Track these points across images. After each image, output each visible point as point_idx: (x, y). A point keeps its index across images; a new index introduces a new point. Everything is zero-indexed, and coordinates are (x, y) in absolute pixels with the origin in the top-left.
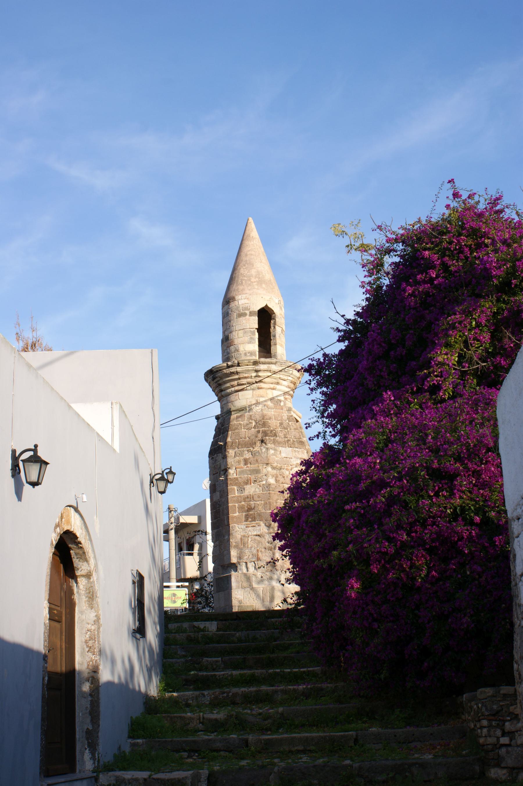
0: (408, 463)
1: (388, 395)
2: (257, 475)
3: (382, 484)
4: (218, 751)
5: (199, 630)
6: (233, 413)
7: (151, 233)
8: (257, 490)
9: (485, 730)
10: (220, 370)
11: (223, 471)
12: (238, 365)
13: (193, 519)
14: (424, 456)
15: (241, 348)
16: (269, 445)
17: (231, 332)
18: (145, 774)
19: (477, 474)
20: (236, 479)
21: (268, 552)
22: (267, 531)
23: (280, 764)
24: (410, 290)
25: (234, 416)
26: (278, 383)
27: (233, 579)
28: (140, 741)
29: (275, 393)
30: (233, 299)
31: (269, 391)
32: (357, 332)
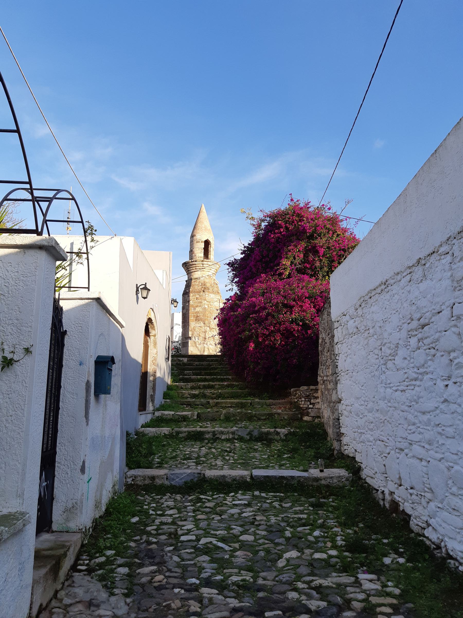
0: (276, 301)
1: (263, 275)
3: (265, 308)
4: (198, 405)
5: (180, 361)
7: (152, 209)
9: (303, 402)
12: (196, 261)
14: (280, 299)
15: (197, 255)
18: (173, 413)
19: (301, 306)
23: (224, 411)
24: (272, 236)
28: (168, 400)
29: (210, 273)
30: (195, 235)
31: (207, 272)
32: (249, 252)
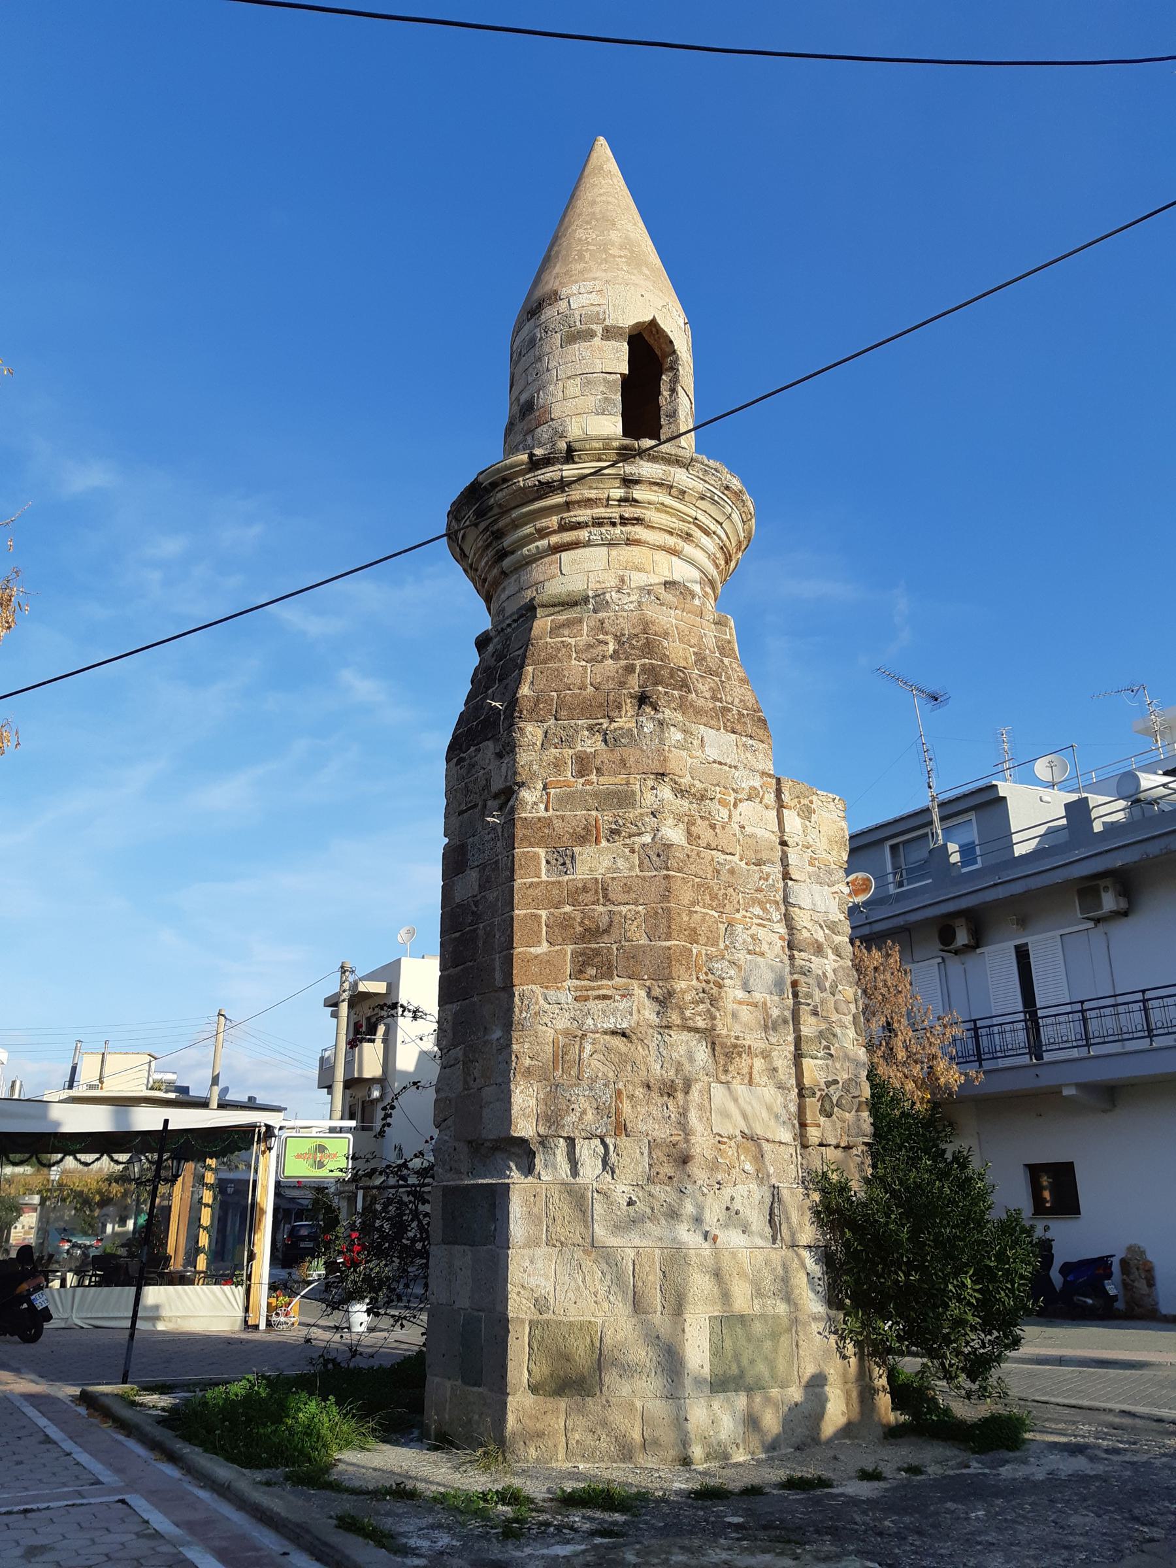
2: (621, 812)
6: (540, 612)
7: (362, 687)
8: (621, 863)
10: (505, 480)
11: (496, 796)
12: (570, 456)
13: (379, 987)
16: (667, 711)
17: (542, 387)
20: (548, 823)
21: (660, 1101)
22: (653, 1018)
25: (542, 624)
26: (687, 537)
27: (516, 1208)
31: (661, 556)
